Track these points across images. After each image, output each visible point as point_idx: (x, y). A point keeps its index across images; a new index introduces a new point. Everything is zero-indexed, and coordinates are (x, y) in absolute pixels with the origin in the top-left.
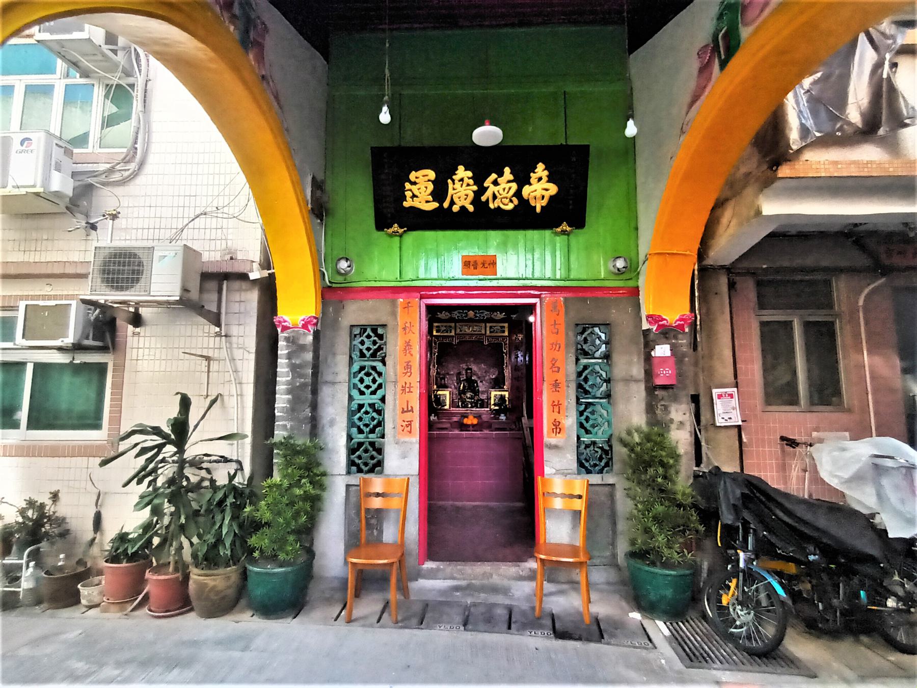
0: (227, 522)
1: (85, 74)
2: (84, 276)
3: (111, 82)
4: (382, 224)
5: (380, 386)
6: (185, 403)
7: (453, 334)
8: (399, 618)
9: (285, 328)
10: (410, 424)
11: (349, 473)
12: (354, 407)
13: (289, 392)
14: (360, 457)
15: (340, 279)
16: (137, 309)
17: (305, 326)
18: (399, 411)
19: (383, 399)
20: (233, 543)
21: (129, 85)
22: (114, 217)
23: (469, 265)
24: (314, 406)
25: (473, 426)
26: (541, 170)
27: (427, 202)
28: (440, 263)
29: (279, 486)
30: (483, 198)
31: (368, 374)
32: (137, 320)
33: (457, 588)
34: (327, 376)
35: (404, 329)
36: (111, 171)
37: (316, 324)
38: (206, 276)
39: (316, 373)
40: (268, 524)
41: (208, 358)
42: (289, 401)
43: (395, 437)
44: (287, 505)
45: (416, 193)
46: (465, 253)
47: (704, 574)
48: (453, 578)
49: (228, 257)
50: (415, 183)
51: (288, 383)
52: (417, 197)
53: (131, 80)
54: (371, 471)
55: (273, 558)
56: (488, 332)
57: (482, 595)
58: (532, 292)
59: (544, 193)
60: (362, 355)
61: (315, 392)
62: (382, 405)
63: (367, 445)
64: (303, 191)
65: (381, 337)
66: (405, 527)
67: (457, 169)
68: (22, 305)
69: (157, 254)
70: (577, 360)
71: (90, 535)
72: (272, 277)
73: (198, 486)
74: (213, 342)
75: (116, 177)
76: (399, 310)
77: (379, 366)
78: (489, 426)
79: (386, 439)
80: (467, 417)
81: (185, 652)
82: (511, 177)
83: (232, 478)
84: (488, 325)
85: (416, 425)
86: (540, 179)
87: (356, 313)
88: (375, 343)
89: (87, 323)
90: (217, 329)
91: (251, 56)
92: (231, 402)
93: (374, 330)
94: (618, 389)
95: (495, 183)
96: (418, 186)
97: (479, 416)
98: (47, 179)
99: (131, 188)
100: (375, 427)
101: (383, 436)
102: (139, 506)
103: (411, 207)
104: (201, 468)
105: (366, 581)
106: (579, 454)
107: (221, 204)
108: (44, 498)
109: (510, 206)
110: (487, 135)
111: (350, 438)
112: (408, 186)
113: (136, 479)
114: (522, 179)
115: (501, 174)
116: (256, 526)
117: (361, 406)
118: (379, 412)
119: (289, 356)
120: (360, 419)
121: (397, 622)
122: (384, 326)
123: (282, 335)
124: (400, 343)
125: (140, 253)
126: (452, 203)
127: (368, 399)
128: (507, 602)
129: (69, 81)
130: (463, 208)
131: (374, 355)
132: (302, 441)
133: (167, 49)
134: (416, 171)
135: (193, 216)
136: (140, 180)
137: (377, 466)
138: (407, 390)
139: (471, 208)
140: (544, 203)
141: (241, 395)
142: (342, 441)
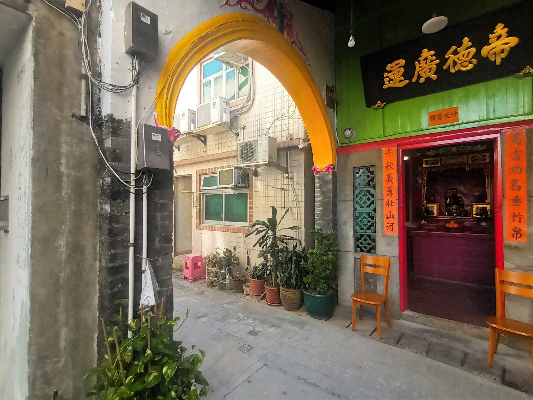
0: (293, 268)
1: (232, 66)
2: (235, 156)
3: (239, 67)
4: (370, 103)
5: (372, 202)
6: (274, 211)
7: (439, 165)
8: (383, 337)
9: (318, 172)
11: (355, 251)
13: (321, 206)
14: (361, 243)
16: (256, 169)
17: (327, 170)
19: (374, 210)
20: (296, 279)
21: (246, 65)
22: (244, 128)
23: (434, 118)
24: (335, 213)
25: (454, 228)
26: (500, 29)
27: (400, 81)
28: (416, 120)
29: (316, 254)
30: (445, 67)
32: (256, 174)
33: (427, 331)
34: (341, 197)
35: (387, 167)
36: (242, 108)
37: (334, 168)
38: (279, 150)
39: (335, 196)
40: (312, 272)
41: (284, 190)
42: (321, 211)
43: (382, 233)
44: (320, 264)
45: (392, 77)
46: (432, 110)
47: (304, 291)
48: (426, 325)
49: (289, 138)
50: (391, 72)
51: (320, 201)
52: (392, 80)
53: (247, 62)
54: (369, 251)
55: (315, 289)
56: (470, 161)
57: (446, 340)
58: (491, 129)
59: (504, 47)
61: (335, 206)
62: (374, 213)
63: (366, 237)
64: (321, 96)
65: (372, 173)
66: (392, 286)
67: (422, 53)
68: (218, 170)
69: (259, 143)
71: (247, 266)
72: (310, 145)
73: (282, 251)
74: (288, 181)
75: (245, 110)
76: (383, 155)
77: (372, 190)
78: (470, 229)
79: (377, 234)
80: (449, 222)
81: (276, 322)
82: (470, 44)
83: (295, 247)
84: (470, 156)
85: (396, 226)
86: (499, 37)
87: (356, 159)
89: (239, 176)
90: (287, 175)
91: (285, 34)
92: (295, 211)
93: (368, 168)
95: (455, 53)
96: (393, 73)
98: (221, 118)
99: (250, 113)
100: (370, 226)
102: (260, 256)
103: (389, 88)
104: (283, 242)
105: (363, 313)
107: (283, 113)
108: (231, 249)
109: (471, 66)
110: (434, 24)
111: (355, 231)
112: (385, 74)
113: (258, 244)
115: (460, 44)
116: (307, 273)
118: (373, 218)
119: (320, 187)
120: (361, 221)
121: (381, 339)
123: (316, 176)
124: (385, 177)
125: (253, 143)
128: (466, 349)
129: (227, 71)
130: (428, 79)
132: (327, 231)
133: (247, 49)
134: (391, 63)
135: (273, 120)
136: (254, 108)
137: (372, 249)
138: (390, 204)
139: (435, 77)
140: (503, 55)
141: (299, 208)
142: (351, 233)
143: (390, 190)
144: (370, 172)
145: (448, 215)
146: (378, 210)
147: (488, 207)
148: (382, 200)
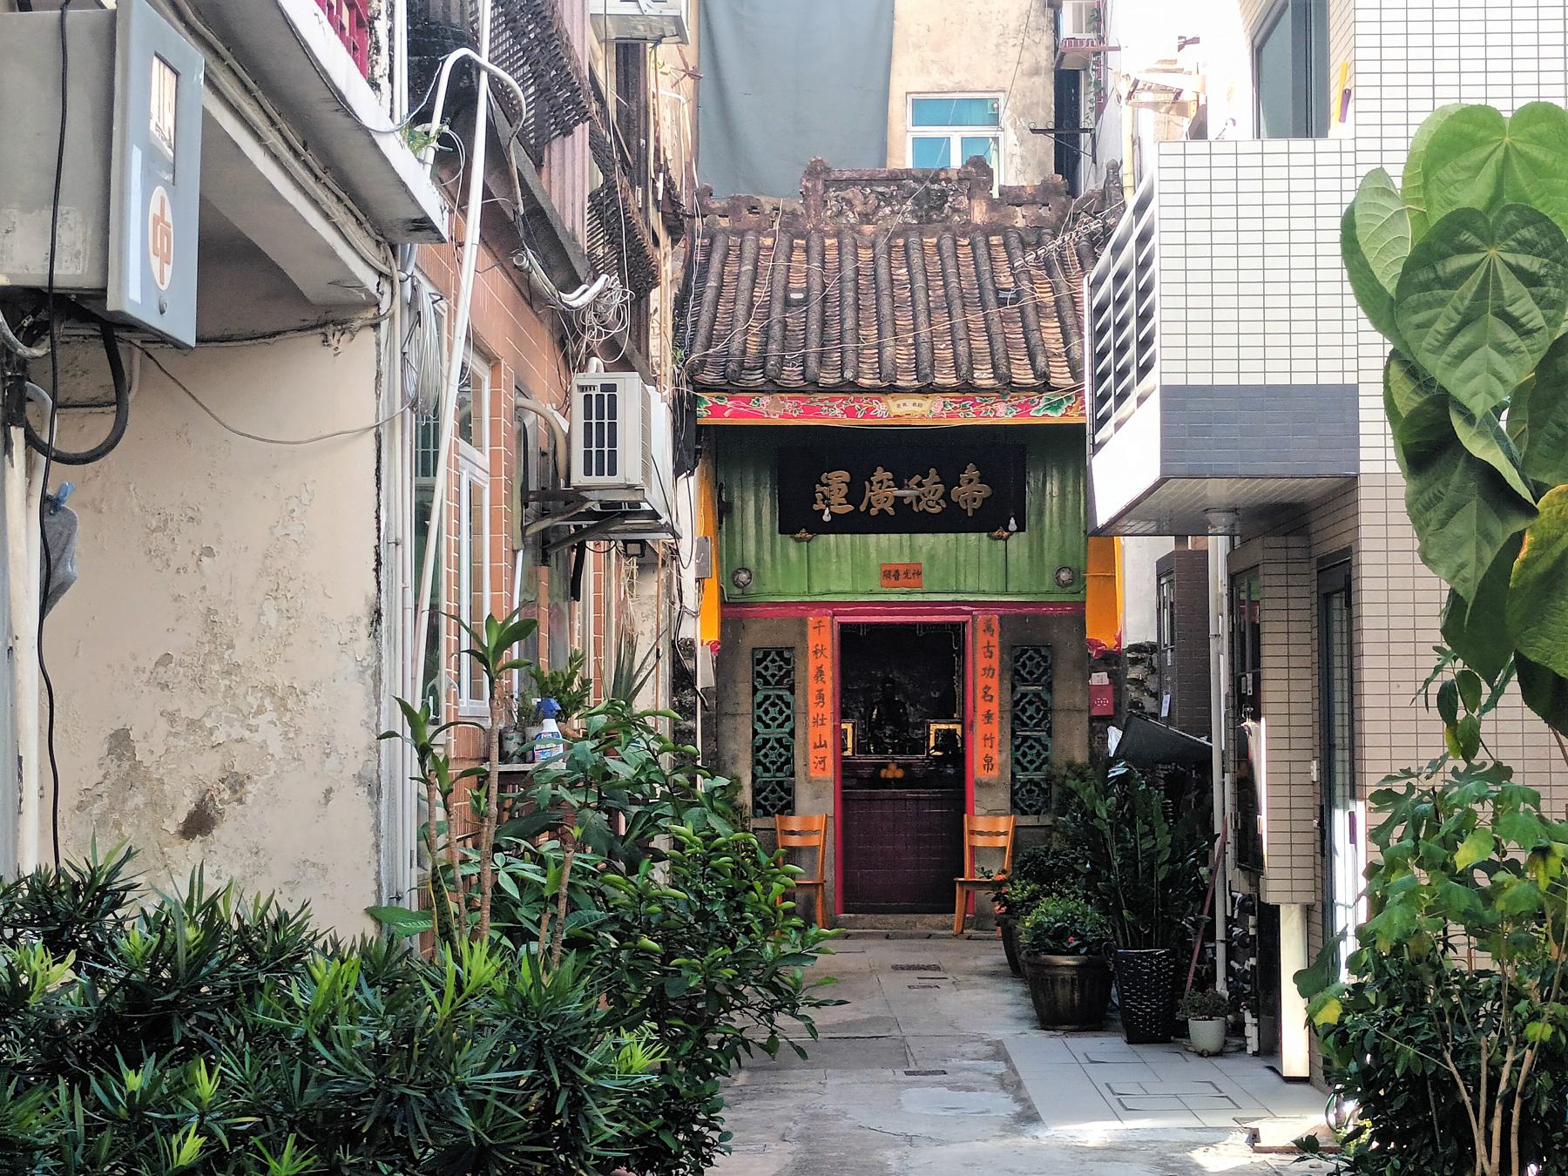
5: (788, 718)
10: (823, 761)
12: (759, 742)
15: (737, 591)
18: (811, 747)
19: (792, 733)
25: (895, 779)
26: (971, 472)
31: (773, 705)
60: (767, 683)
70: (1014, 688)
77: (786, 694)
78: (924, 782)
82: (938, 479)
86: (971, 481)
88: (780, 668)
93: (780, 654)
94: (1059, 720)
97: (906, 767)
100: (783, 764)
101: (793, 774)
106: (1014, 793)
109: (937, 509)
114: (950, 481)
115: (925, 476)
117: (766, 741)
118: (787, 748)
120: (766, 756)
122: (790, 649)
124: (812, 670)
126: (870, 505)
127: (774, 733)
130: (882, 511)
131: (779, 682)
139: (891, 512)
140: (977, 505)
143: (821, 696)
144: (783, 659)
145: (876, 752)
146: (799, 733)
147: (958, 728)
148: (806, 714)
